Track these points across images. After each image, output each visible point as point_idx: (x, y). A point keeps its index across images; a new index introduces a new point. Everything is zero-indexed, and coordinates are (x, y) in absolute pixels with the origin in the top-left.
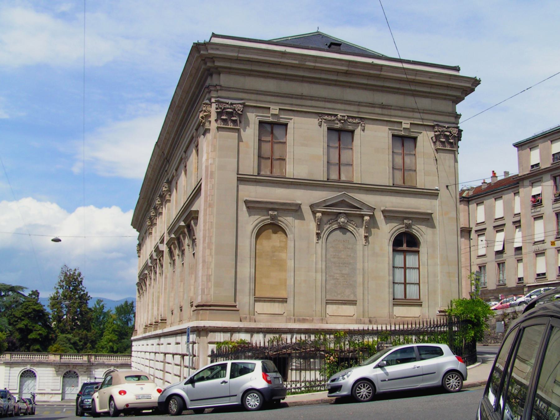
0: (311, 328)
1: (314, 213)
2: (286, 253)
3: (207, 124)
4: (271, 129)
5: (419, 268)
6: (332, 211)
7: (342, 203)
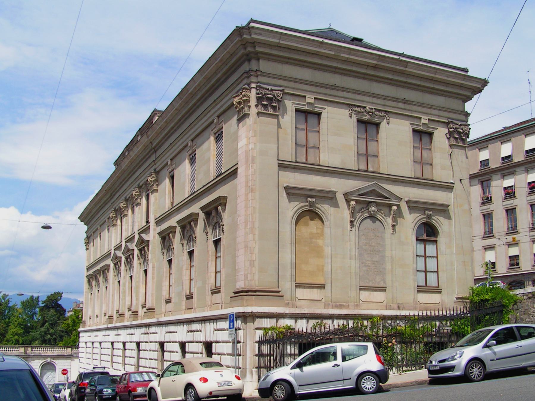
0: (350, 313)
1: (348, 201)
3: (246, 108)
4: (309, 116)
5: (437, 257)
7: (373, 193)
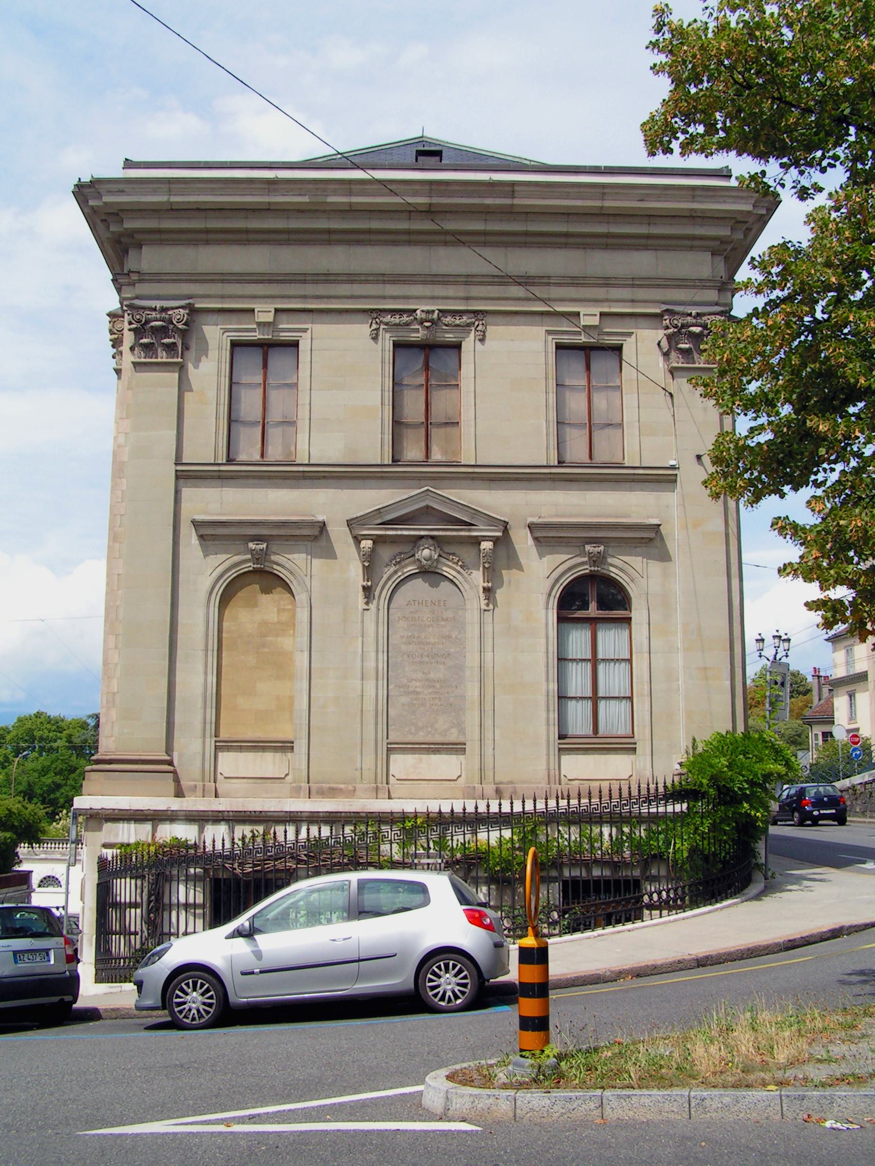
1: (357, 540)
2: (294, 636)
5: (630, 661)
6: (399, 533)
7: (426, 514)
